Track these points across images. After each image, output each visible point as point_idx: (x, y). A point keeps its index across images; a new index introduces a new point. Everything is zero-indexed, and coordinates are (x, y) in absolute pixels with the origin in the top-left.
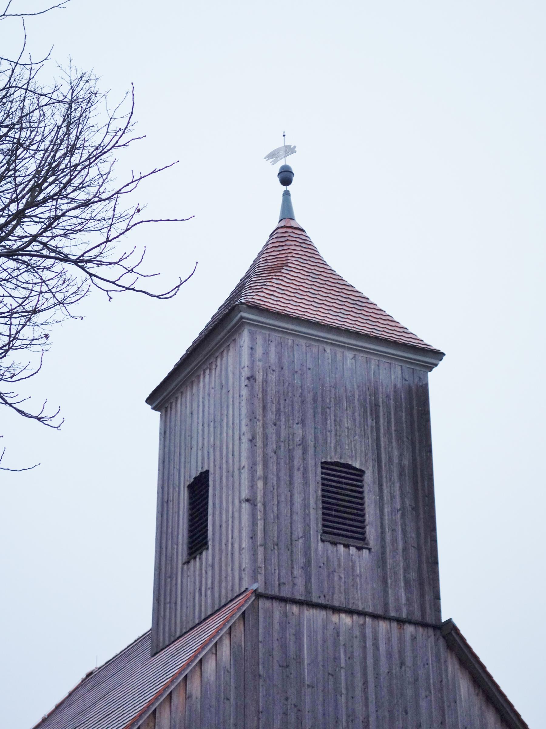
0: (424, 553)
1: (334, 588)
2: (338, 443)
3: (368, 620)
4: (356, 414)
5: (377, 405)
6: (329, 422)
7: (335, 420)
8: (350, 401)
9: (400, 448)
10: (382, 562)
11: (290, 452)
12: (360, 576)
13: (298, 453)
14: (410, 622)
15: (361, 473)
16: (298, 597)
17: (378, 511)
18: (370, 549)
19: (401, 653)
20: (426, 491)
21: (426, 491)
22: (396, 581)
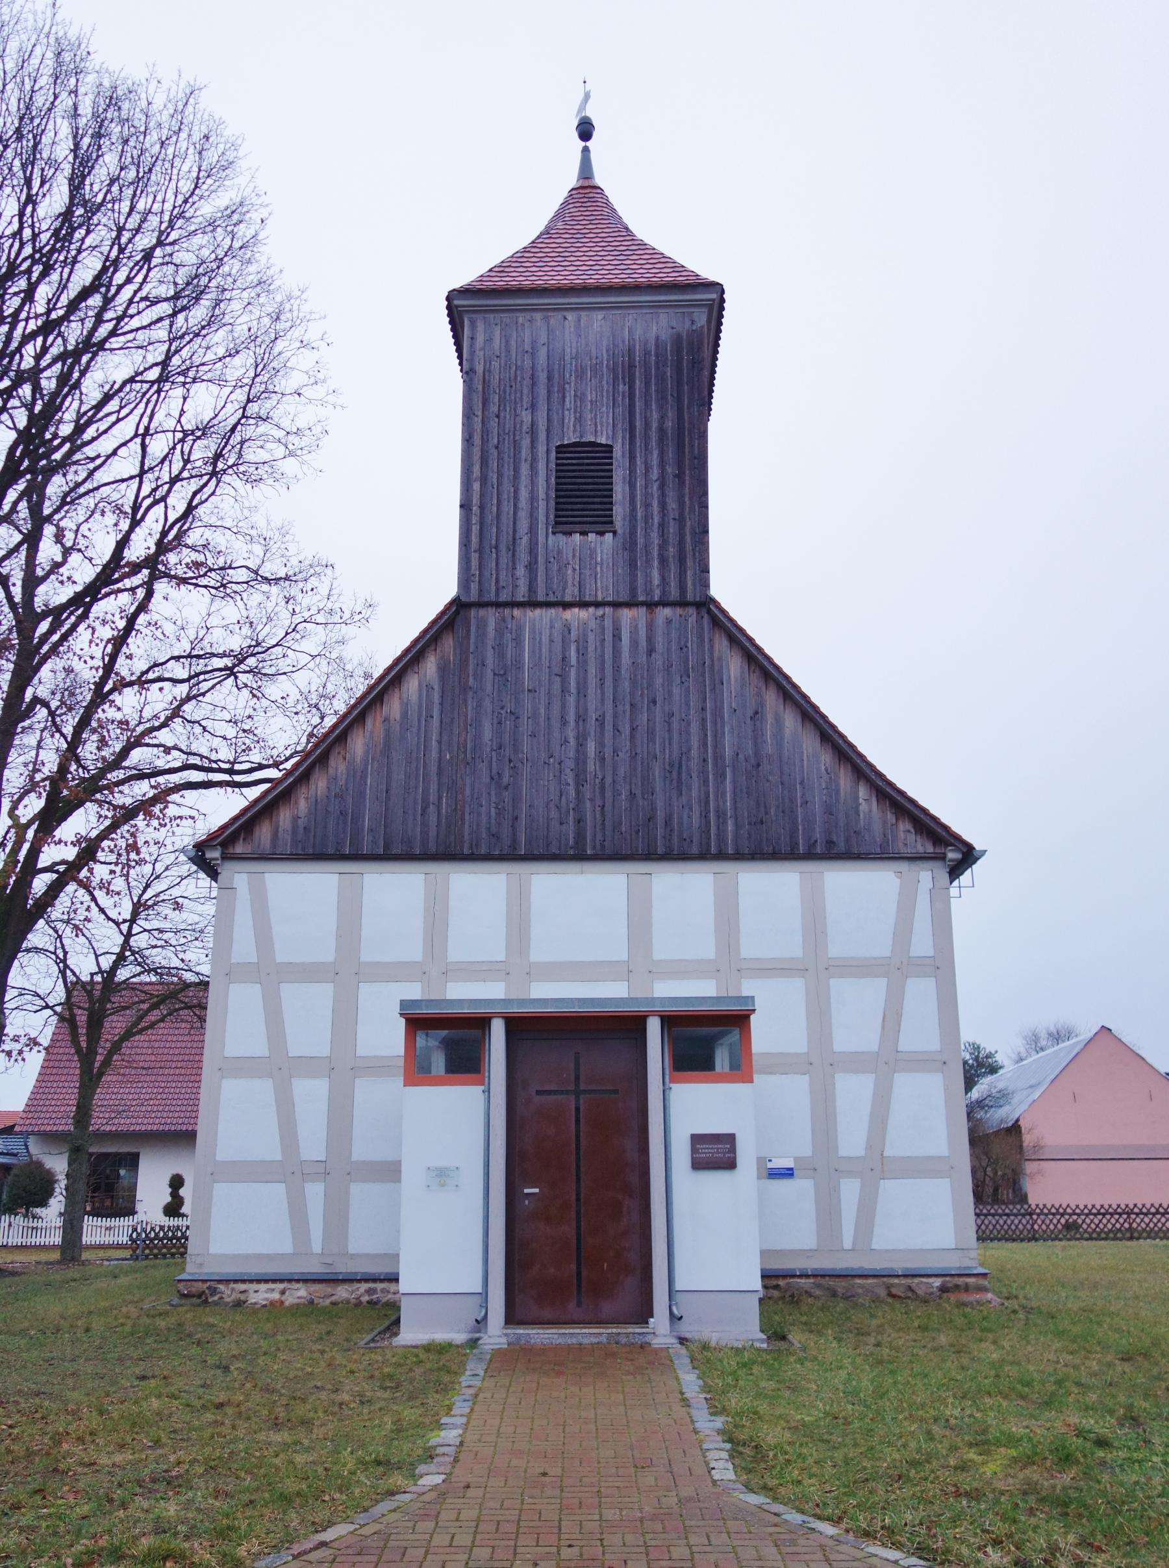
0: (688, 523)
1: (566, 582)
2: (579, 420)
3: (608, 610)
4: (604, 382)
5: (632, 366)
6: (567, 400)
7: (575, 396)
8: (595, 370)
9: (661, 409)
10: (630, 545)
11: (516, 445)
12: (602, 564)
13: (526, 442)
14: (665, 604)
15: (609, 449)
16: (520, 598)
17: (627, 488)
18: (615, 533)
19: (650, 639)
20: (696, 452)
21: (696, 452)
22: (648, 562)
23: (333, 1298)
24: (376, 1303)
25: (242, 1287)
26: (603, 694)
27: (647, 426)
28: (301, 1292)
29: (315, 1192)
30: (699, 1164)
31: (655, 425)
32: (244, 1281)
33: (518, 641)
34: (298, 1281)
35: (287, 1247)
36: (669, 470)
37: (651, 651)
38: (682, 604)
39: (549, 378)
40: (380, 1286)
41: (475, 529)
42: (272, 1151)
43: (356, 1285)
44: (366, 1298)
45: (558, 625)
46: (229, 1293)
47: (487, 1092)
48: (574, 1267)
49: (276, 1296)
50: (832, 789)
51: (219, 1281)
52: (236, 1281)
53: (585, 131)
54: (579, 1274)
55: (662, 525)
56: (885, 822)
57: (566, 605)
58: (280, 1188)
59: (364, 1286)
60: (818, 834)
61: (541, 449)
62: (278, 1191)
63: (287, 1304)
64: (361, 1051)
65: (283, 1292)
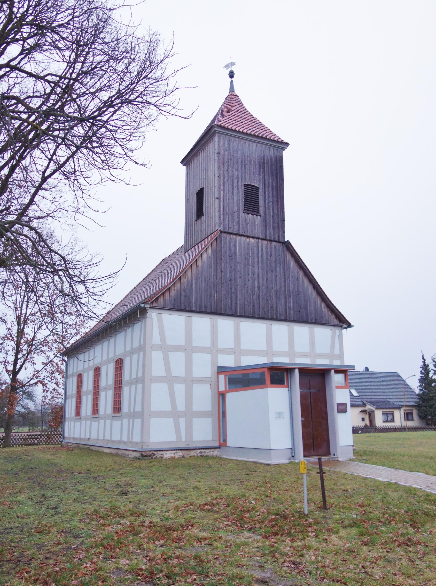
8: (254, 162)
10: (265, 220)
13: (235, 181)
14: (274, 241)
18: (261, 216)
19: (271, 252)
23: (190, 455)
24: (203, 456)
25: (162, 452)
26: (259, 267)
27: (269, 184)
28: (180, 453)
29: (182, 421)
30: (339, 411)
31: (271, 184)
32: (162, 451)
33: (235, 246)
34: (179, 450)
35: (174, 439)
36: (274, 199)
37: (271, 255)
38: (279, 242)
39: (242, 162)
40: (203, 451)
41: (222, 207)
42: (169, 408)
43: (196, 451)
44: (200, 455)
45: (246, 243)
46: (158, 455)
47: (290, 391)
48: (312, 440)
49: (172, 455)
50: (316, 304)
51: (155, 451)
52: (160, 451)
53: (232, 75)
54: (313, 442)
55: (273, 216)
56: (328, 315)
57: (249, 237)
58: (171, 420)
59: (199, 451)
60: (313, 316)
61: (240, 184)
62: (171, 421)
63: (176, 457)
64: (194, 375)
65: (174, 454)
